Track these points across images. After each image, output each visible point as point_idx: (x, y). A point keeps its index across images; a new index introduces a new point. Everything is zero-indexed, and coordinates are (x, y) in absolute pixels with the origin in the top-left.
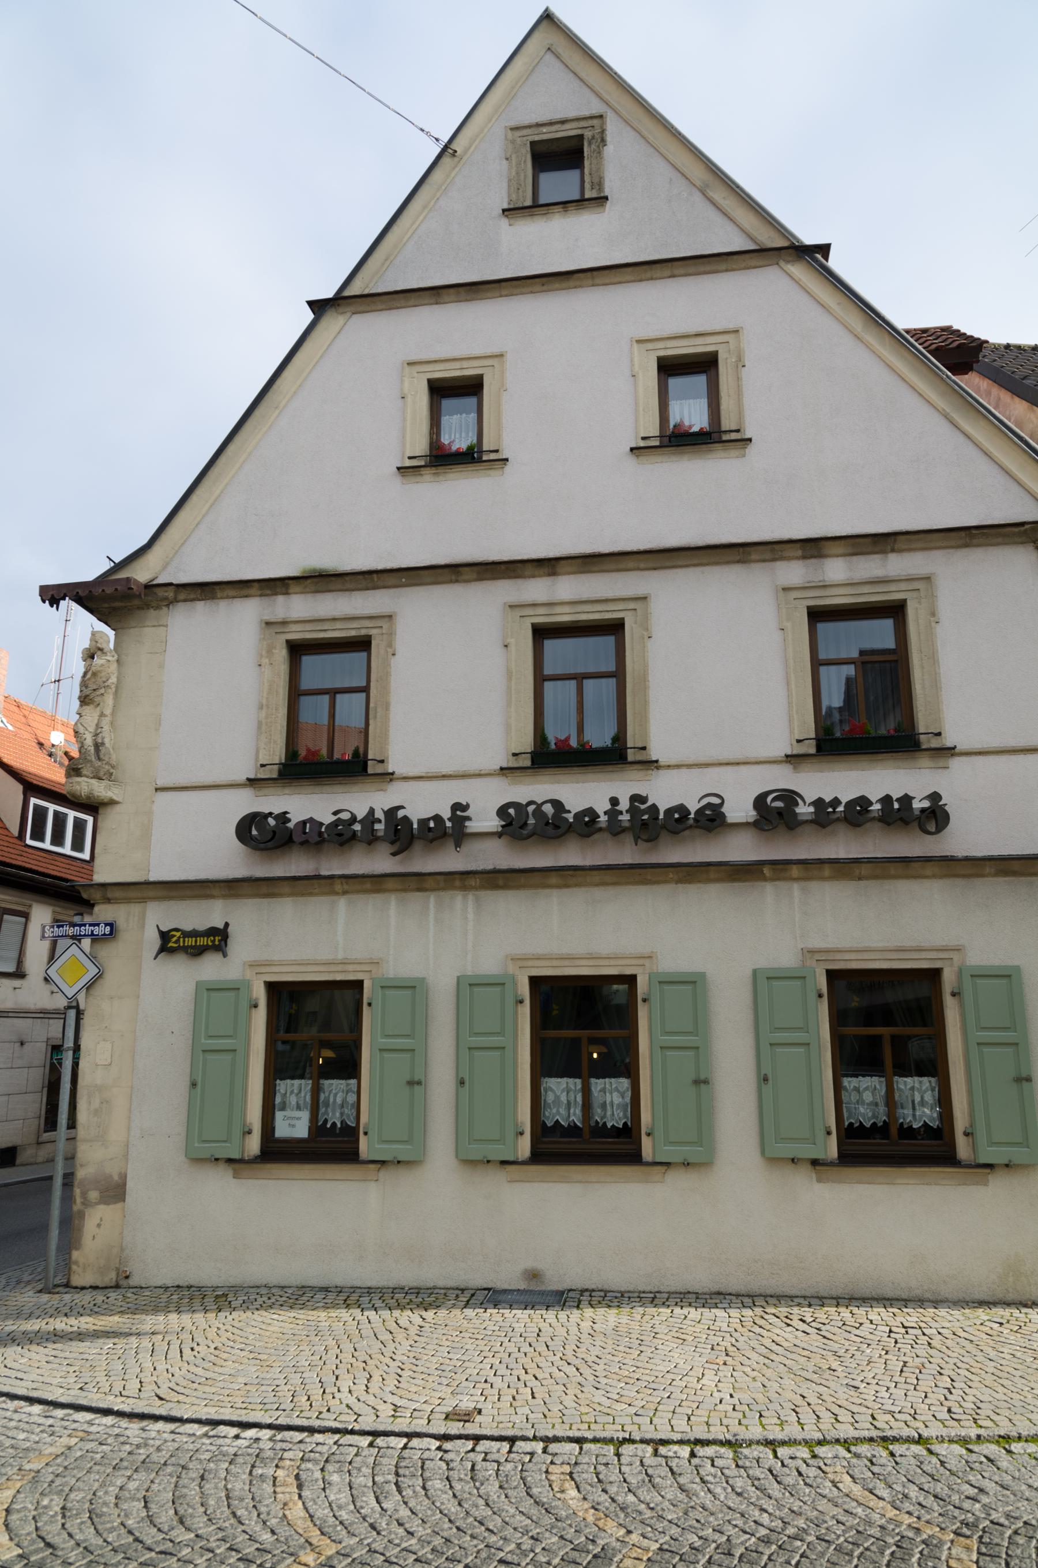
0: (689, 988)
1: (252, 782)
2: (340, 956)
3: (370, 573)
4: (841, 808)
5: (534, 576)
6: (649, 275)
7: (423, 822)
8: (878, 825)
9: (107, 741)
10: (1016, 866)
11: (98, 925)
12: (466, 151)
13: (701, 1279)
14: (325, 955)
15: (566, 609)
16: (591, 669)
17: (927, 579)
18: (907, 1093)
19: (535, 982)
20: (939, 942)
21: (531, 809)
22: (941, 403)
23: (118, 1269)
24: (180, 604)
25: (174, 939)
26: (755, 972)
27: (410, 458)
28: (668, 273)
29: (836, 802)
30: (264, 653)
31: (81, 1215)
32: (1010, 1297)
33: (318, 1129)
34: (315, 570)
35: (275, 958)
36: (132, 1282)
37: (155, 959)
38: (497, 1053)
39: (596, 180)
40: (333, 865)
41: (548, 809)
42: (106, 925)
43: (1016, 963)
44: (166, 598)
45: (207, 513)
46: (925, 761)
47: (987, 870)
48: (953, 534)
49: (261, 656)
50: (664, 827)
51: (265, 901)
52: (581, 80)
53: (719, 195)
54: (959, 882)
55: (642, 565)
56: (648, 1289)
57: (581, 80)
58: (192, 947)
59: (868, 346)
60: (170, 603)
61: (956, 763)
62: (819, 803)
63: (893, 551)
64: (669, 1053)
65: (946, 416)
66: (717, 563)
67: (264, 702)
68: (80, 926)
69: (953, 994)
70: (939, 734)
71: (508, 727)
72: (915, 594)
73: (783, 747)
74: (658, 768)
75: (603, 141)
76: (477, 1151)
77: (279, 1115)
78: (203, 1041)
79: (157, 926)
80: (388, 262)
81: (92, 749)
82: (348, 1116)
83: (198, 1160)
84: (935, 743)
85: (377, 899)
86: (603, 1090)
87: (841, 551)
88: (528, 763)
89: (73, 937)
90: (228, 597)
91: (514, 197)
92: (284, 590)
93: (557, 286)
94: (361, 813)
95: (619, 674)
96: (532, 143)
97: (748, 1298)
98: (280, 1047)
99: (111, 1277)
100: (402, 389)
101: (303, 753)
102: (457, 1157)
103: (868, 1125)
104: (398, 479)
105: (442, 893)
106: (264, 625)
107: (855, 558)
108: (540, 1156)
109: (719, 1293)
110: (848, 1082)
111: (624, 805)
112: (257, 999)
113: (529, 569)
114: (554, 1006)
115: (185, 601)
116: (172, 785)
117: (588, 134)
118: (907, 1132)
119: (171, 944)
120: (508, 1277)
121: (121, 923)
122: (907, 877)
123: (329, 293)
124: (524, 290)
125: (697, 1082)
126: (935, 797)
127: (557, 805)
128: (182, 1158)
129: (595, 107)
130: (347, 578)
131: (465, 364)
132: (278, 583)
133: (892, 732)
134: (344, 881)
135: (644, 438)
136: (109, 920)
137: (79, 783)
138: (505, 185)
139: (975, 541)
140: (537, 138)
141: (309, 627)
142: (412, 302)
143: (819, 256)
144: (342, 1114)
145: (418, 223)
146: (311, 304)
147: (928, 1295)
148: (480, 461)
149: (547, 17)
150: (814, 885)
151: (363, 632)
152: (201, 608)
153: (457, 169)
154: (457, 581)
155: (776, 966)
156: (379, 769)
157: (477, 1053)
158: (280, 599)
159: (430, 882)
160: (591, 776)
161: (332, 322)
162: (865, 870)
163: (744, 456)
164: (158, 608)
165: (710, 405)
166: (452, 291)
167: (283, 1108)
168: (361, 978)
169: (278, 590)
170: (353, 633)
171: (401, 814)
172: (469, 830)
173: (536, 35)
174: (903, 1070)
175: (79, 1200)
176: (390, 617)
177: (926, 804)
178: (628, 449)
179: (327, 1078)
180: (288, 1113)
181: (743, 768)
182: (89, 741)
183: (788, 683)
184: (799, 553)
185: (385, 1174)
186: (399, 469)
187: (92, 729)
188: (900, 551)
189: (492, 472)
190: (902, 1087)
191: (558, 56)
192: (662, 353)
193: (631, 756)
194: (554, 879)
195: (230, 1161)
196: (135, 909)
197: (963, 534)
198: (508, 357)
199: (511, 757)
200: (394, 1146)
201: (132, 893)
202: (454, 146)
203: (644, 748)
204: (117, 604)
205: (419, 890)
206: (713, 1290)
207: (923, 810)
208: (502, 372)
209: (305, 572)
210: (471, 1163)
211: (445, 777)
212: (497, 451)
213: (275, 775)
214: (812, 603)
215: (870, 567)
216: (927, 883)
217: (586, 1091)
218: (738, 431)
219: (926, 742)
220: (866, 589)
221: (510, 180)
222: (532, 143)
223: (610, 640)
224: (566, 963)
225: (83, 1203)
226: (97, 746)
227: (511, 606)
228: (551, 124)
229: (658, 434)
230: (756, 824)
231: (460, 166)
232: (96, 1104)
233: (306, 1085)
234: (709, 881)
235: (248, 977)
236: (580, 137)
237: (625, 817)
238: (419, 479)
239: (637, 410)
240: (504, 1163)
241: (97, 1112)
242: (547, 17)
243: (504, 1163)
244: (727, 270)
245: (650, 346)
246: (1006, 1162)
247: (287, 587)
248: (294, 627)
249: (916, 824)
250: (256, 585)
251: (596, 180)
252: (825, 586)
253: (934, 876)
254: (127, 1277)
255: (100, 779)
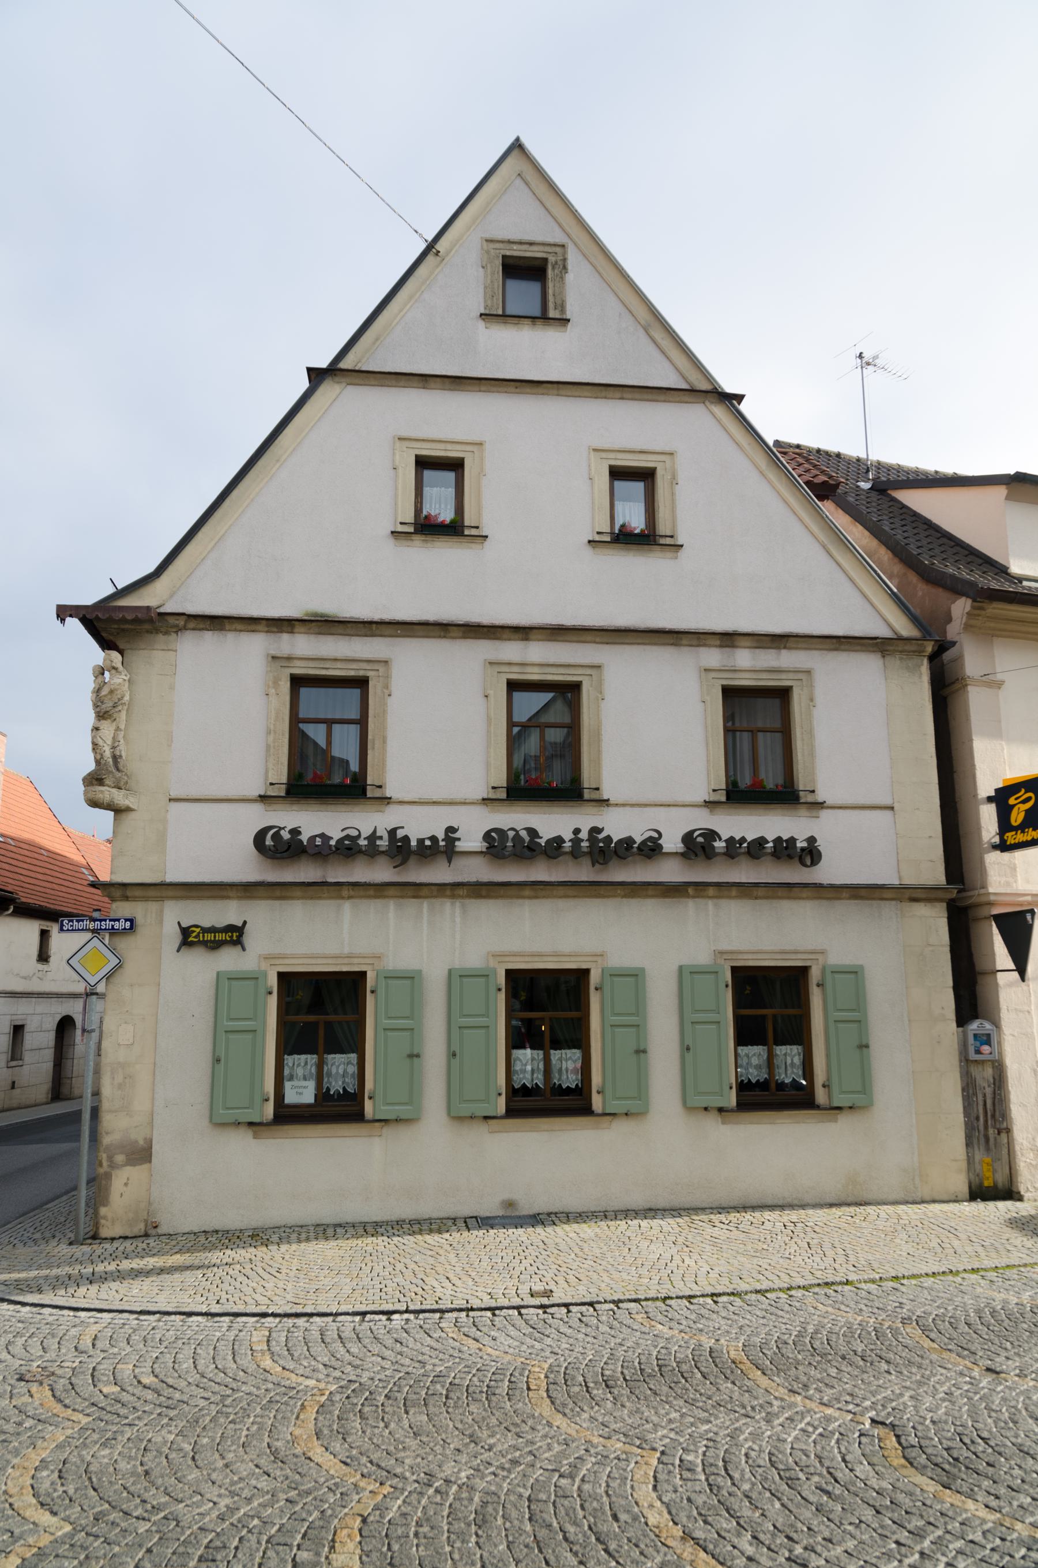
0: (408, 982)
1: (263, 798)
2: (346, 951)
3: (371, 623)
4: (745, 845)
5: (510, 640)
6: (603, 394)
7: (421, 842)
8: (769, 858)
9: (123, 754)
10: (863, 892)
11: (118, 920)
12: (448, 253)
13: (637, 1200)
14: (332, 949)
15: (536, 670)
16: (338, 716)
17: (808, 672)
18: (782, 1057)
19: (734, 970)
20: (810, 947)
21: (511, 834)
22: (822, 537)
23: (146, 1221)
24: (188, 632)
25: (194, 934)
26: (681, 968)
27: (401, 523)
28: (618, 395)
29: (743, 840)
30: (270, 683)
31: (108, 1176)
32: (850, 1200)
33: (323, 1096)
34: (316, 615)
35: (288, 952)
36: (160, 1231)
37: (178, 951)
38: (483, 1031)
39: (559, 302)
40: (337, 874)
41: (524, 834)
42: (126, 920)
43: (860, 963)
44: (177, 626)
45: (212, 549)
46: (803, 811)
47: (844, 895)
48: (828, 640)
49: (269, 687)
50: (415, 853)
51: (277, 903)
52: (547, 210)
53: (659, 335)
54: (825, 902)
55: (598, 640)
56: (597, 1209)
57: (547, 210)
58: (211, 941)
59: (769, 482)
60: (178, 630)
61: (824, 814)
62: (731, 841)
63: (785, 648)
64: (617, 1030)
65: (824, 547)
66: (655, 644)
67: (272, 727)
68: (101, 921)
69: (818, 985)
70: (813, 791)
71: (488, 764)
72: (799, 683)
73: (702, 794)
74: (608, 805)
75: (565, 268)
76: (466, 1109)
77: (288, 1085)
78: (225, 1023)
79: (179, 923)
80: (378, 343)
81: (110, 760)
82: (348, 1084)
83: (220, 1124)
84: (810, 798)
85: (379, 903)
86: (560, 1059)
87: (748, 644)
88: (504, 796)
89: (94, 931)
90: (236, 630)
91: (489, 303)
92: (289, 629)
93: (528, 390)
94: (366, 832)
95: (362, 722)
96: (504, 257)
97: (675, 1211)
98: (514, 1023)
99: (140, 1228)
100: (393, 461)
101: (309, 776)
102: (211, 1121)
103: (754, 1081)
104: (391, 541)
105: (433, 900)
106: (270, 659)
107: (757, 651)
108: (511, 1112)
109: (650, 1209)
110: (740, 1049)
111: (584, 835)
112: (271, 987)
113: (507, 634)
114: (523, 994)
115: (194, 629)
116: (186, 797)
117: (552, 259)
118: (781, 1086)
119: (191, 939)
120: (490, 1207)
121: (139, 920)
122: (789, 898)
123: (324, 364)
124: (500, 389)
125: (411, 1056)
126: (812, 840)
127: (533, 832)
128: (205, 1122)
129: (559, 237)
130: (349, 625)
131: (449, 447)
132: (286, 623)
133: (781, 789)
134: (350, 887)
135: (598, 533)
136: (128, 916)
137: (102, 792)
138: (482, 291)
139: (842, 647)
140: (508, 253)
141: (311, 664)
142: (401, 384)
143: (735, 402)
144: (343, 1082)
145: (405, 311)
146: (310, 370)
147: (796, 1202)
148: (462, 534)
149: (517, 146)
150: (724, 903)
151: (361, 673)
152: (209, 638)
153: (440, 268)
154: (444, 637)
155: (695, 963)
156: (378, 793)
157: (466, 1031)
158: (285, 636)
159: (425, 891)
160: (555, 809)
161: (328, 390)
162: (761, 892)
163: (676, 558)
164: (166, 633)
165: (646, 511)
166: (438, 379)
167: (291, 1078)
168: (364, 969)
169: (285, 629)
170: (352, 673)
171: (400, 834)
172: (457, 849)
173: (509, 161)
174: (557, 1045)
175: (105, 1163)
176: (386, 662)
177: (805, 844)
178: (586, 541)
179: (329, 1053)
180: (295, 1083)
181: (673, 809)
182: (108, 754)
183: (707, 744)
184: (718, 643)
185: (387, 1131)
186: (392, 532)
187: (109, 742)
188: (790, 648)
189: (473, 545)
190: (778, 1052)
191: (527, 184)
192: (613, 463)
193: (587, 795)
194: (527, 892)
195: (251, 1124)
196: (153, 906)
197: (834, 641)
198: (487, 446)
199: (491, 790)
200: (397, 1108)
201: (151, 893)
202: (440, 246)
203: (597, 789)
204: (127, 626)
205: (414, 897)
206: (646, 1207)
207: (803, 849)
208: (482, 459)
209: (307, 615)
210: (458, 1117)
211: (435, 803)
212: (477, 527)
213: (283, 794)
214: (725, 682)
215: (768, 658)
216: (802, 903)
217: (771, 1057)
218: (672, 537)
219: (804, 797)
220: (764, 676)
221: (485, 287)
222: (504, 257)
223: (356, 692)
224: (536, 959)
225: (110, 1166)
226: (115, 758)
227: (490, 663)
228: (521, 243)
229: (413, 521)
230: (683, 855)
231: (442, 265)
232: (119, 1079)
233: (312, 1059)
234: (647, 896)
235: (263, 968)
236: (546, 260)
237: (585, 844)
238: (409, 543)
239: (593, 509)
240: (486, 1118)
241: (120, 1086)
242: (517, 146)
243: (486, 1118)
244: (665, 401)
245: (604, 455)
246: (850, 1105)
247: (293, 627)
248: (298, 663)
249: (797, 859)
250: (264, 622)
251: (559, 302)
252: (735, 671)
253: (808, 898)
254: (156, 1227)
255: (120, 788)
